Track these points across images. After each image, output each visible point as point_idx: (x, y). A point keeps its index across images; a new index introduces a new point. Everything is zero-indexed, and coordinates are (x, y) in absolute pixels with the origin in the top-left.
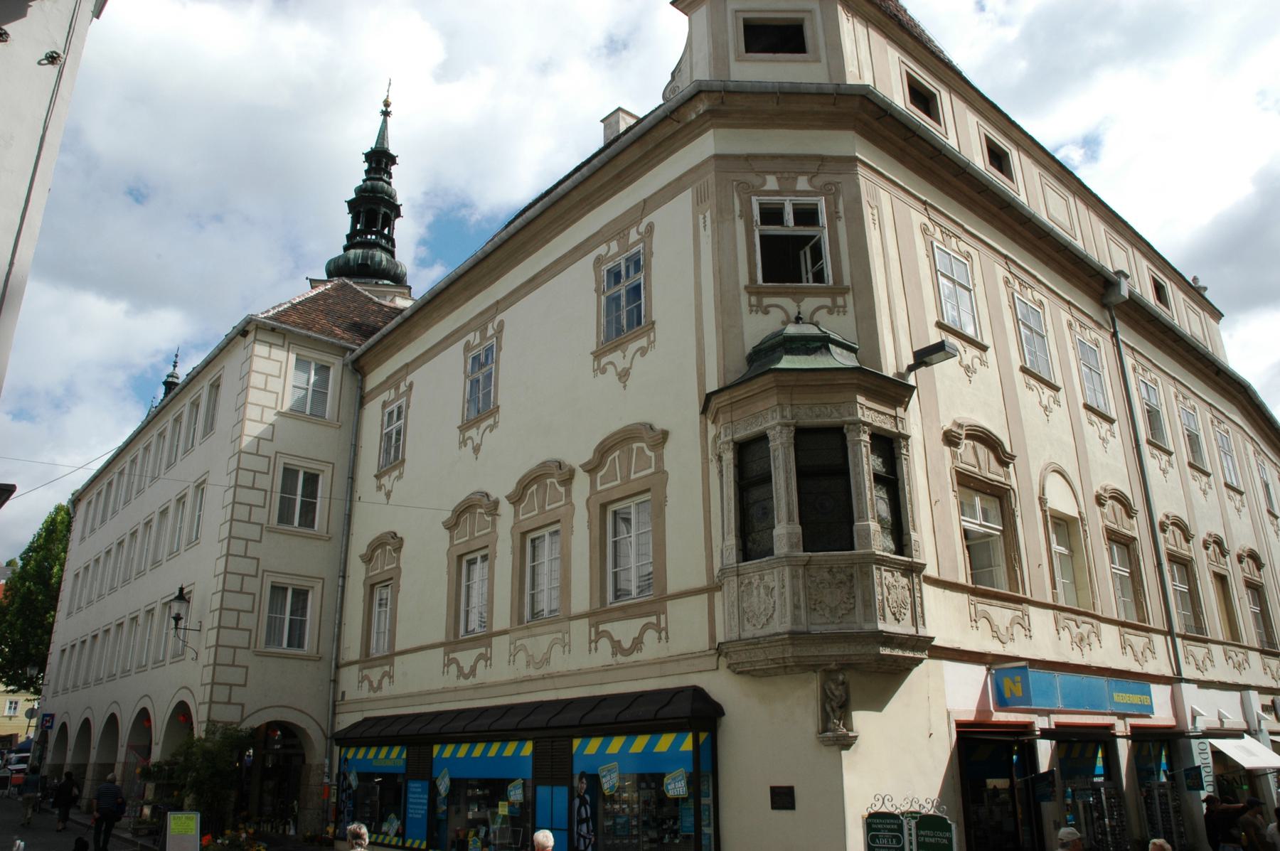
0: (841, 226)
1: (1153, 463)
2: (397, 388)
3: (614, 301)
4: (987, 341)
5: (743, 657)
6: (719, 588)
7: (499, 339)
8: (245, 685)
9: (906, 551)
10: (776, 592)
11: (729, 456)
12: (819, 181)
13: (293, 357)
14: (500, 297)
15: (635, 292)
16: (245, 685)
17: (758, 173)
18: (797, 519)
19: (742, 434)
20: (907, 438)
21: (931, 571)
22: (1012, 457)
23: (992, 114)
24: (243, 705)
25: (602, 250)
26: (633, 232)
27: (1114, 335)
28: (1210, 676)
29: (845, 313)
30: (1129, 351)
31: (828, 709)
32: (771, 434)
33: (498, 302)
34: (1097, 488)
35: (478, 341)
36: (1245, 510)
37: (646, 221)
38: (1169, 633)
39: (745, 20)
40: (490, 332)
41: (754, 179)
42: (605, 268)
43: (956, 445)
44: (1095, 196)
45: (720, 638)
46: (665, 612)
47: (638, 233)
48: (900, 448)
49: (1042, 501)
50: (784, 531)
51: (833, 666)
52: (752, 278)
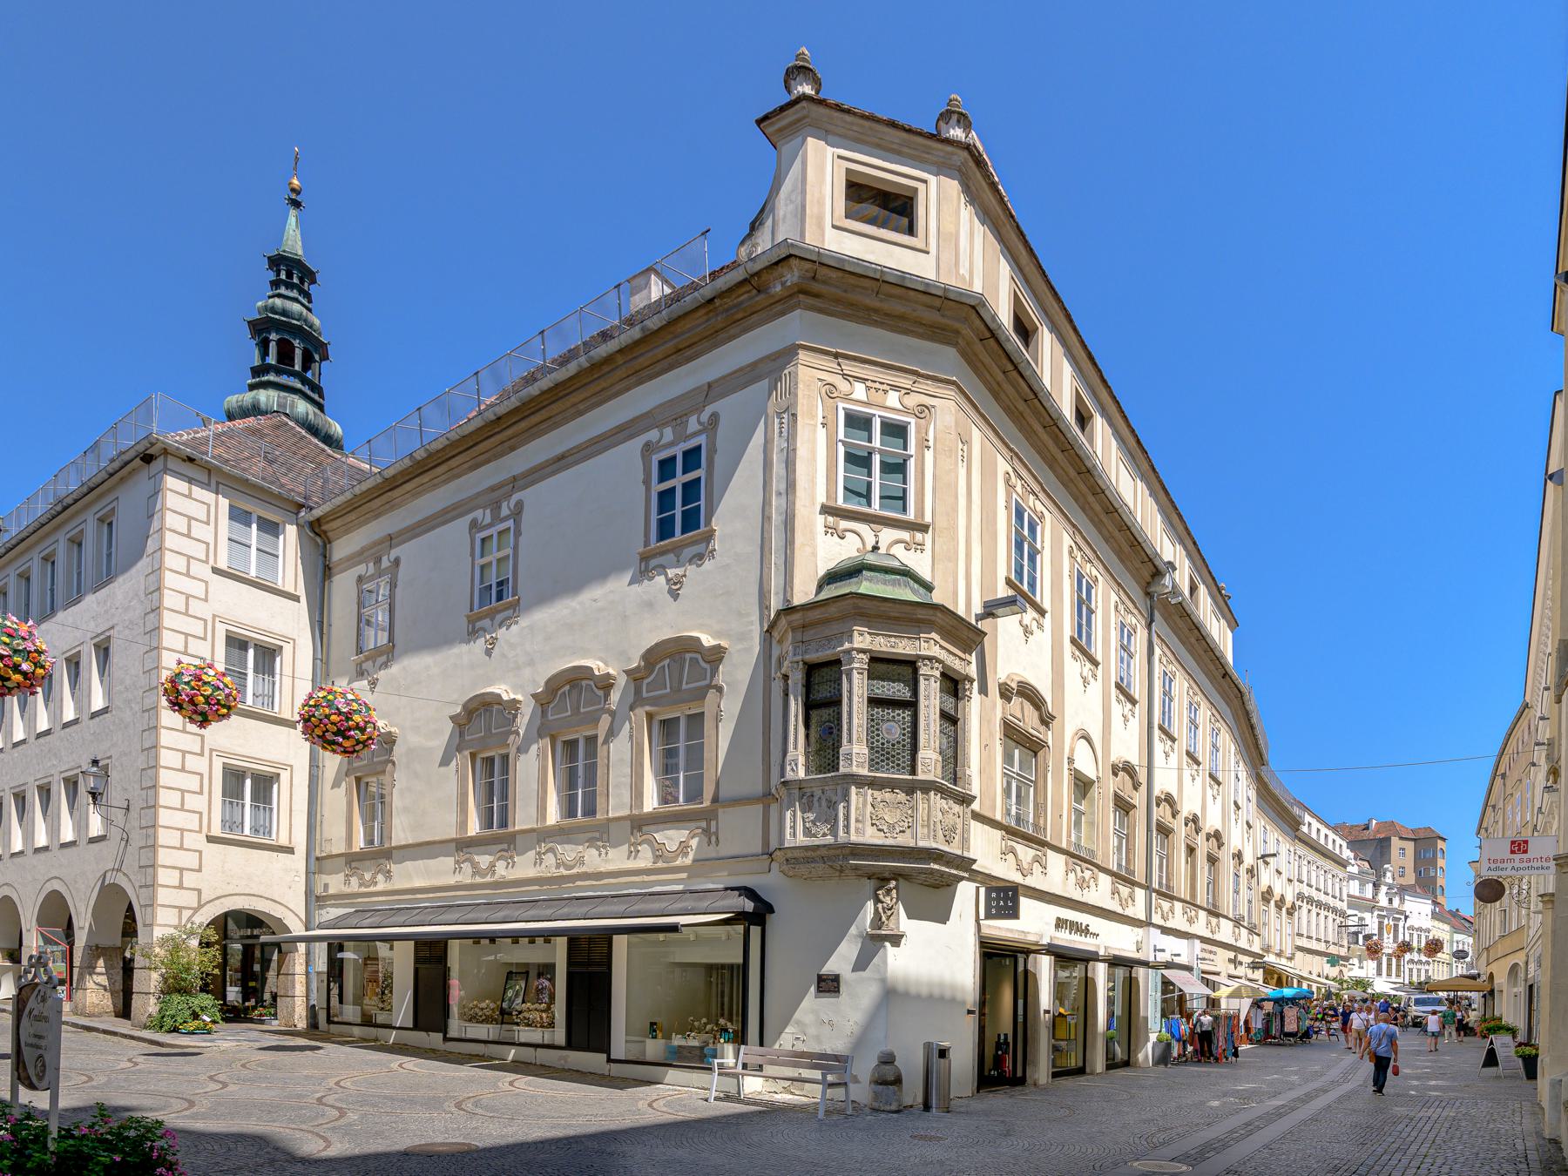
0: (929, 455)
1: (1159, 747)
2: (378, 561)
3: (666, 498)
7: (517, 523)
8: (200, 870)
13: (224, 503)
14: (517, 471)
15: (691, 489)
16: (200, 870)
22: (1053, 718)
24: (199, 891)
25: (653, 435)
26: (693, 420)
28: (1169, 924)
33: (515, 478)
34: (1114, 758)
35: (488, 520)
36: (1219, 798)
37: (709, 410)
38: (1147, 887)
40: (505, 511)
41: (843, 386)
42: (656, 459)
43: (1009, 700)
46: (716, 818)
47: (699, 422)
49: (1071, 761)
51: (886, 875)
52: (831, 492)
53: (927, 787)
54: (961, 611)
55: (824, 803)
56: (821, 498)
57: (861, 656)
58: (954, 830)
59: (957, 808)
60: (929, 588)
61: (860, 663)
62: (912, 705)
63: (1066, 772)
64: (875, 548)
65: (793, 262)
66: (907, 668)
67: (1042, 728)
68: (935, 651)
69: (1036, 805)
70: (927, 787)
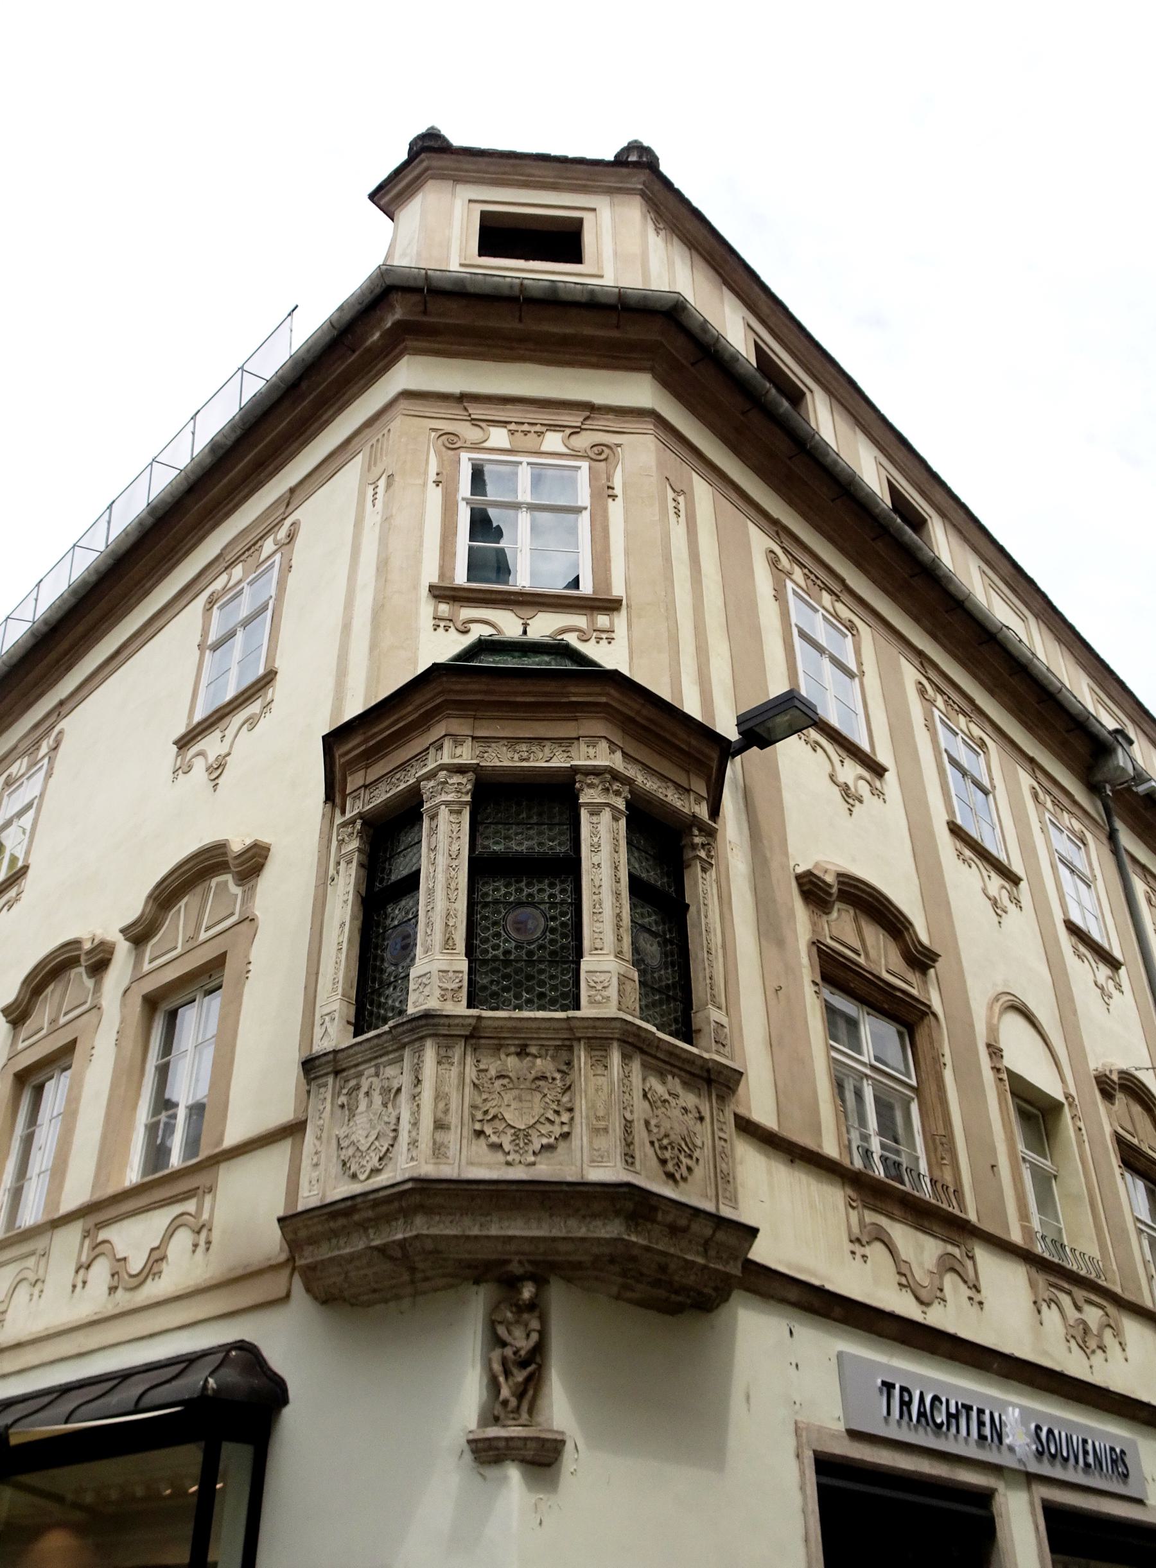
0: (616, 510)
4: (884, 757)
10: (404, 1097)
12: (583, 441)
17: (475, 422)
18: (461, 946)
21: (760, 1102)
23: (900, 454)
27: (1112, 837)
29: (610, 640)
30: (1138, 870)
34: (1095, 1063)
39: (484, 214)
44: (1071, 627)
49: (995, 1052)
53: (600, 1037)
55: (377, 1099)
56: (430, 575)
57: (456, 779)
61: (458, 790)
62: (567, 868)
63: (988, 1075)
65: (396, 297)
66: (558, 796)
67: (912, 977)
68: (601, 756)
69: (931, 1140)
70: (600, 1037)
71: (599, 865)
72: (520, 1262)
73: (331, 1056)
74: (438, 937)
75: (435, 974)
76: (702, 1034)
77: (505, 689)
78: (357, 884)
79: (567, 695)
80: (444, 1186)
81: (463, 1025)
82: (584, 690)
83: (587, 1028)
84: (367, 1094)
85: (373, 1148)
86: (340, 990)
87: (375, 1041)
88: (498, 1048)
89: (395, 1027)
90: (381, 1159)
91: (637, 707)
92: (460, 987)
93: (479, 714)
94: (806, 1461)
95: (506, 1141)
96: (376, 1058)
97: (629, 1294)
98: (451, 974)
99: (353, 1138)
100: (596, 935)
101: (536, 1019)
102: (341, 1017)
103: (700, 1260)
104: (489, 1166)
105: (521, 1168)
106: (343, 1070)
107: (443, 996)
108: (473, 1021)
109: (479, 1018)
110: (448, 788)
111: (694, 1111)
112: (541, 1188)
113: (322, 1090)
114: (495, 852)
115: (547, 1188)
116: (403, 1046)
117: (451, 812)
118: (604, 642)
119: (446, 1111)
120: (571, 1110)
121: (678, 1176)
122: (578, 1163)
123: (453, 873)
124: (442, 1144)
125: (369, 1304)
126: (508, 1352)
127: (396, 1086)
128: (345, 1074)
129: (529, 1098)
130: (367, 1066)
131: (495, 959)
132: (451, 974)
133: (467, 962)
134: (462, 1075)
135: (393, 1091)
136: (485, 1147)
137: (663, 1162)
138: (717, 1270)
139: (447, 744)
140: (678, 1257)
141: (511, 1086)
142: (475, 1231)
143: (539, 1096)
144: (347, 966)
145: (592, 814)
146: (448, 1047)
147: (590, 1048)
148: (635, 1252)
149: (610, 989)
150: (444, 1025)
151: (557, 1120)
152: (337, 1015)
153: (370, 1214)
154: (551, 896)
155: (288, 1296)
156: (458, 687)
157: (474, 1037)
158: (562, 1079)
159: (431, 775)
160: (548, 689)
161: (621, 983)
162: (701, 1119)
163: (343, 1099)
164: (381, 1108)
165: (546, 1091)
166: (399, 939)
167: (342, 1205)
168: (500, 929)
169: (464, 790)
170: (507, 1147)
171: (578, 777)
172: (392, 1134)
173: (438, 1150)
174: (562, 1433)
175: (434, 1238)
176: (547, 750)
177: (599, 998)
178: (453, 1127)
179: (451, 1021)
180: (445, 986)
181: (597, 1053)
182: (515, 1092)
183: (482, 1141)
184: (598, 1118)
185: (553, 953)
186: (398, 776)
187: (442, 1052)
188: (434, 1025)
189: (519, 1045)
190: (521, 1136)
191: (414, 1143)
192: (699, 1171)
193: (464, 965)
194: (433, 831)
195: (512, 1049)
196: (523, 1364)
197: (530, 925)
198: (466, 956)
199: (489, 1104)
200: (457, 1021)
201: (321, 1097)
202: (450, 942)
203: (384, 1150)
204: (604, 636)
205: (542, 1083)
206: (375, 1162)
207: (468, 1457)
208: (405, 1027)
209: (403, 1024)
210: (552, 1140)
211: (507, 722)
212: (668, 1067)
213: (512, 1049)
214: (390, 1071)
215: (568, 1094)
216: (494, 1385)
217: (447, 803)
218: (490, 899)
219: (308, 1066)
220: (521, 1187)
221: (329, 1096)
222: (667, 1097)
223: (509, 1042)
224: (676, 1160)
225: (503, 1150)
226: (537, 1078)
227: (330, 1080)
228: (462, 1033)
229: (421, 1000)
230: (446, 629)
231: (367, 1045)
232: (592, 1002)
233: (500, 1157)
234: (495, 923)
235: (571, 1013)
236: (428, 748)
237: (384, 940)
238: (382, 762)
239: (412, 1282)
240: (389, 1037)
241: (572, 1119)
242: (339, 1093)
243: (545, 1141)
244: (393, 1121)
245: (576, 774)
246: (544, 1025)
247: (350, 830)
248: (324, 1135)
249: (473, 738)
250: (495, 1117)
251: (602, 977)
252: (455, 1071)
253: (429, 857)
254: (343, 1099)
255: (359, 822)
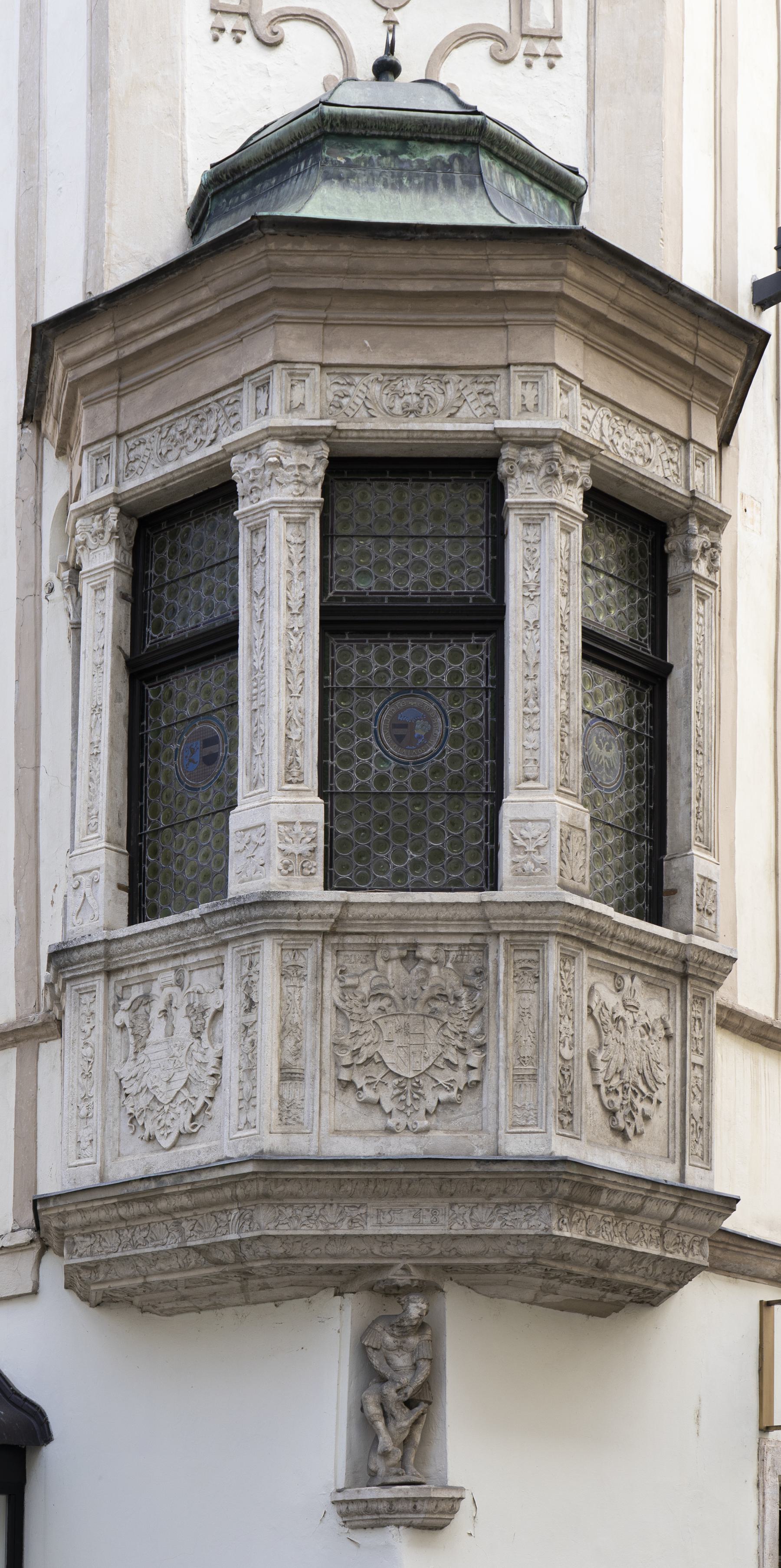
5: (111, 1247)
6: (53, 1027)
9: (675, 910)
10: (229, 1025)
11: (103, 558)
19: (154, 469)
20: (717, 521)
29: (552, 58)
31: (373, 1409)
32: (243, 469)
43: (610, 589)
45: (49, 1184)
48: (688, 556)
50: (274, 817)
54: (696, 276)
55: (182, 1024)
57: (293, 457)
58: (643, 1085)
59: (653, 1007)
60: (564, 186)
62: (484, 619)
64: (386, 69)
70: (531, 930)
71: (536, 624)
72: (405, 1268)
73: (100, 949)
74: (276, 763)
75: (274, 828)
76: (677, 898)
77: (381, 265)
78: (116, 634)
79: (492, 276)
80: (301, 1168)
81: (320, 917)
82: (521, 266)
83: (511, 918)
84: (165, 1013)
85: (180, 1099)
86: (102, 831)
87: (176, 932)
88: (373, 950)
89: (210, 915)
90: (193, 1118)
91: (611, 291)
92: (313, 851)
93: (332, 314)
94: (768, 1491)
95: (386, 1096)
96: (176, 956)
97: (549, 1298)
98: (298, 828)
99: (147, 1081)
100: (527, 755)
101: (432, 904)
102: (108, 879)
103: (654, 1250)
104: (361, 1133)
105: (409, 1138)
106: (121, 970)
107: (286, 866)
108: (335, 910)
109: (346, 904)
110: (283, 475)
111: (659, 1027)
112: (441, 1168)
113: (87, 998)
114: (360, 596)
115: (450, 1168)
116: (225, 943)
117: (288, 522)
118: (540, 64)
119: (297, 1052)
120: (482, 1047)
121: (630, 1132)
122: (491, 1129)
123: (295, 641)
124: (292, 1104)
125: (170, 1313)
126: (390, 1391)
127: (213, 1007)
128: (123, 976)
129: (420, 1029)
130: (162, 967)
131: (364, 792)
132: (298, 828)
133: (322, 807)
134: (319, 996)
135: (210, 1014)
136: (354, 1105)
137: (612, 1113)
138: (674, 1261)
139: (278, 378)
140: (624, 1250)
141: (392, 1010)
142: (343, 1229)
143: (434, 1025)
144: (111, 788)
145: (528, 523)
146: (296, 951)
147: (514, 946)
148: (569, 1249)
149: (546, 850)
150: (290, 917)
151: (462, 1063)
152: (102, 876)
153: (185, 1201)
154: (456, 675)
155: (35, 1292)
156: (298, 262)
157: (336, 931)
158: (470, 1000)
159: (251, 446)
160: (456, 265)
161: (566, 839)
162: (669, 1038)
163: (122, 1017)
164: (192, 1039)
165: (445, 1018)
166: (199, 744)
167: (142, 1187)
168: (370, 738)
169: (310, 480)
170: (387, 1106)
171: (508, 452)
172: (212, 1082)
173: (287, 1112)
174: (462, 1489)
175: (284, 1239)
176: (451, 390)
177: (529, 866)
178: (307, 1077)
179: (302, 911)
180: (289, 848)
181: (523, 956)
182: (400, 1021)
183: (350, 1096)
184: (522, 1060)
185: (456, 780)
186: (182, 425)
187: (288, 959)
188: (276, 917)
189: (403, 946)
190: (408, 1088)
191: (248, 1101)
192: (659, 1119)
193: (316, 810)
194: (260, 556)
195: (395, 952)
196: (410, 1404)
197: (419, 731)
198: (321, 795)
199: (361, 1041)
200: (311, 910)
201: (84, 1009)
202: (295, 771)
203: (199, 1104)
204: (541, 48)
205: (439, 1005)
206: (184, 1122)
207: (334, 1519)
208: (228, 917)
209: (224, 911)
210: (454, 1094)
211: (381, 332)
212: (626, 965)
213: (395, 952)
214: (200, 980)
215: (477, 1021)
216: (364, 1426)
217: (281, 506)
218: (353, 683)
219: (62, 960)
220: (411, 1168)
221: (99, 1008)
222: (621, 1012)
223: (390, 940)
224: (627, 1110)
225: (382, 1109)
226: (433, 998)
227: (99, 982)
228: (319, 928)
229: (250, 871)
230: (237, 36)
231: (161, 937)
232: (520, 873)
233: (377, 1120)
234: (363, 729)
235: (487, 896)
236: (240, 381)
237: (168, 739)
238: (149, 391)
239: (243, 1289)
240: (201, 927)
241: (484, 1060)
242: (116, 1009)
243: (443, 1096)
244: (213, 1062)
245: (503, 444)
246: (444, 913)
247: (96, 525)
248: (97, 1071)
249: (323, 366)
250: (370, 1060)
251: (534, 830)
252: (308, 988)
253: (252, 609)
254: (122, 1017)
255: (113, 512)
